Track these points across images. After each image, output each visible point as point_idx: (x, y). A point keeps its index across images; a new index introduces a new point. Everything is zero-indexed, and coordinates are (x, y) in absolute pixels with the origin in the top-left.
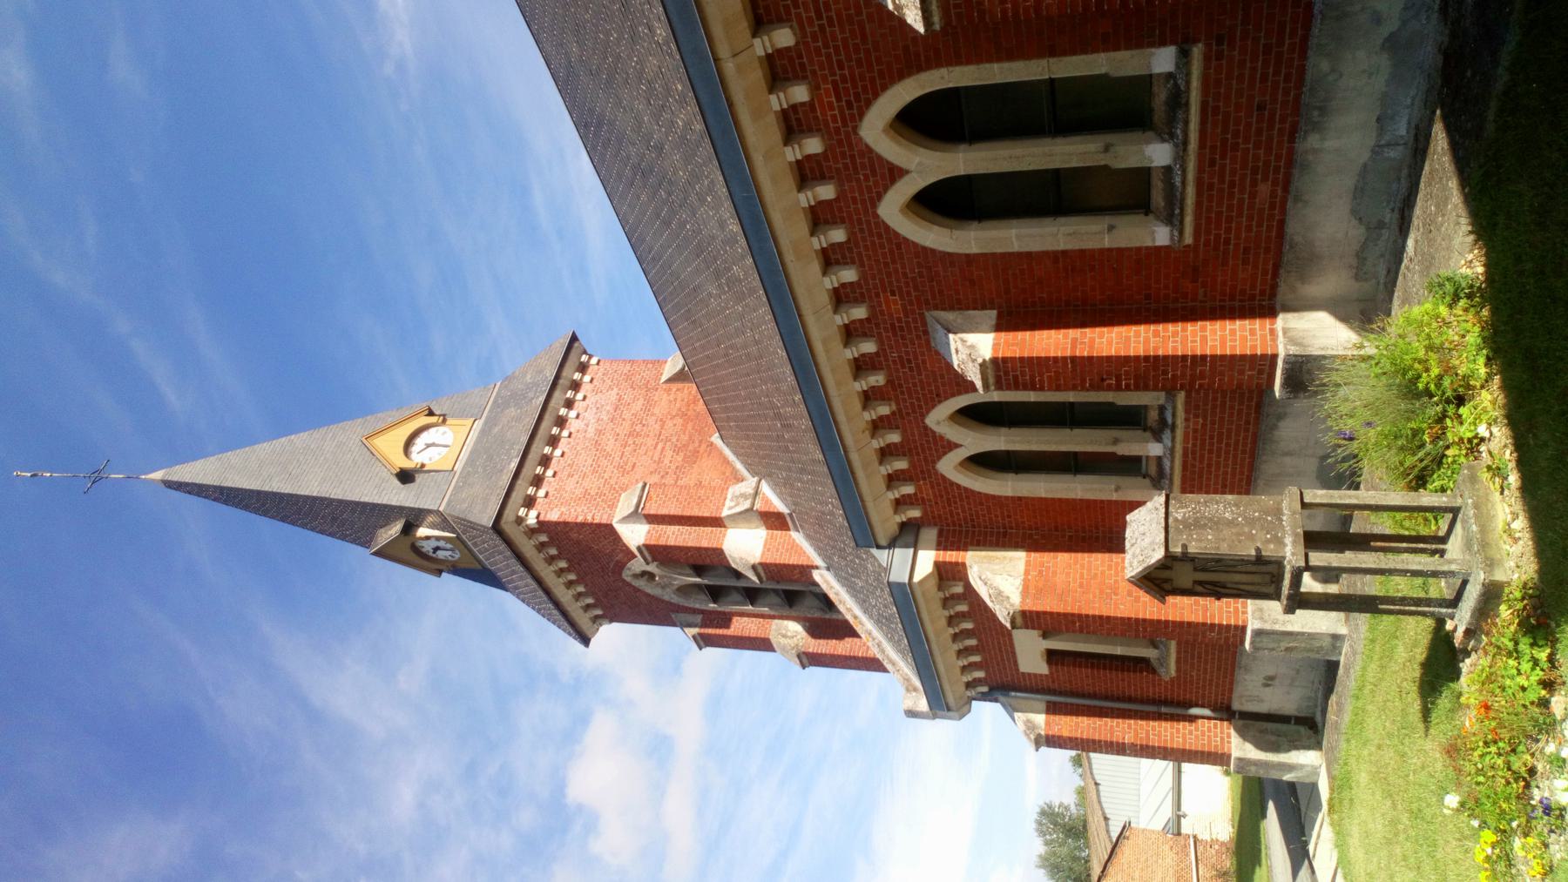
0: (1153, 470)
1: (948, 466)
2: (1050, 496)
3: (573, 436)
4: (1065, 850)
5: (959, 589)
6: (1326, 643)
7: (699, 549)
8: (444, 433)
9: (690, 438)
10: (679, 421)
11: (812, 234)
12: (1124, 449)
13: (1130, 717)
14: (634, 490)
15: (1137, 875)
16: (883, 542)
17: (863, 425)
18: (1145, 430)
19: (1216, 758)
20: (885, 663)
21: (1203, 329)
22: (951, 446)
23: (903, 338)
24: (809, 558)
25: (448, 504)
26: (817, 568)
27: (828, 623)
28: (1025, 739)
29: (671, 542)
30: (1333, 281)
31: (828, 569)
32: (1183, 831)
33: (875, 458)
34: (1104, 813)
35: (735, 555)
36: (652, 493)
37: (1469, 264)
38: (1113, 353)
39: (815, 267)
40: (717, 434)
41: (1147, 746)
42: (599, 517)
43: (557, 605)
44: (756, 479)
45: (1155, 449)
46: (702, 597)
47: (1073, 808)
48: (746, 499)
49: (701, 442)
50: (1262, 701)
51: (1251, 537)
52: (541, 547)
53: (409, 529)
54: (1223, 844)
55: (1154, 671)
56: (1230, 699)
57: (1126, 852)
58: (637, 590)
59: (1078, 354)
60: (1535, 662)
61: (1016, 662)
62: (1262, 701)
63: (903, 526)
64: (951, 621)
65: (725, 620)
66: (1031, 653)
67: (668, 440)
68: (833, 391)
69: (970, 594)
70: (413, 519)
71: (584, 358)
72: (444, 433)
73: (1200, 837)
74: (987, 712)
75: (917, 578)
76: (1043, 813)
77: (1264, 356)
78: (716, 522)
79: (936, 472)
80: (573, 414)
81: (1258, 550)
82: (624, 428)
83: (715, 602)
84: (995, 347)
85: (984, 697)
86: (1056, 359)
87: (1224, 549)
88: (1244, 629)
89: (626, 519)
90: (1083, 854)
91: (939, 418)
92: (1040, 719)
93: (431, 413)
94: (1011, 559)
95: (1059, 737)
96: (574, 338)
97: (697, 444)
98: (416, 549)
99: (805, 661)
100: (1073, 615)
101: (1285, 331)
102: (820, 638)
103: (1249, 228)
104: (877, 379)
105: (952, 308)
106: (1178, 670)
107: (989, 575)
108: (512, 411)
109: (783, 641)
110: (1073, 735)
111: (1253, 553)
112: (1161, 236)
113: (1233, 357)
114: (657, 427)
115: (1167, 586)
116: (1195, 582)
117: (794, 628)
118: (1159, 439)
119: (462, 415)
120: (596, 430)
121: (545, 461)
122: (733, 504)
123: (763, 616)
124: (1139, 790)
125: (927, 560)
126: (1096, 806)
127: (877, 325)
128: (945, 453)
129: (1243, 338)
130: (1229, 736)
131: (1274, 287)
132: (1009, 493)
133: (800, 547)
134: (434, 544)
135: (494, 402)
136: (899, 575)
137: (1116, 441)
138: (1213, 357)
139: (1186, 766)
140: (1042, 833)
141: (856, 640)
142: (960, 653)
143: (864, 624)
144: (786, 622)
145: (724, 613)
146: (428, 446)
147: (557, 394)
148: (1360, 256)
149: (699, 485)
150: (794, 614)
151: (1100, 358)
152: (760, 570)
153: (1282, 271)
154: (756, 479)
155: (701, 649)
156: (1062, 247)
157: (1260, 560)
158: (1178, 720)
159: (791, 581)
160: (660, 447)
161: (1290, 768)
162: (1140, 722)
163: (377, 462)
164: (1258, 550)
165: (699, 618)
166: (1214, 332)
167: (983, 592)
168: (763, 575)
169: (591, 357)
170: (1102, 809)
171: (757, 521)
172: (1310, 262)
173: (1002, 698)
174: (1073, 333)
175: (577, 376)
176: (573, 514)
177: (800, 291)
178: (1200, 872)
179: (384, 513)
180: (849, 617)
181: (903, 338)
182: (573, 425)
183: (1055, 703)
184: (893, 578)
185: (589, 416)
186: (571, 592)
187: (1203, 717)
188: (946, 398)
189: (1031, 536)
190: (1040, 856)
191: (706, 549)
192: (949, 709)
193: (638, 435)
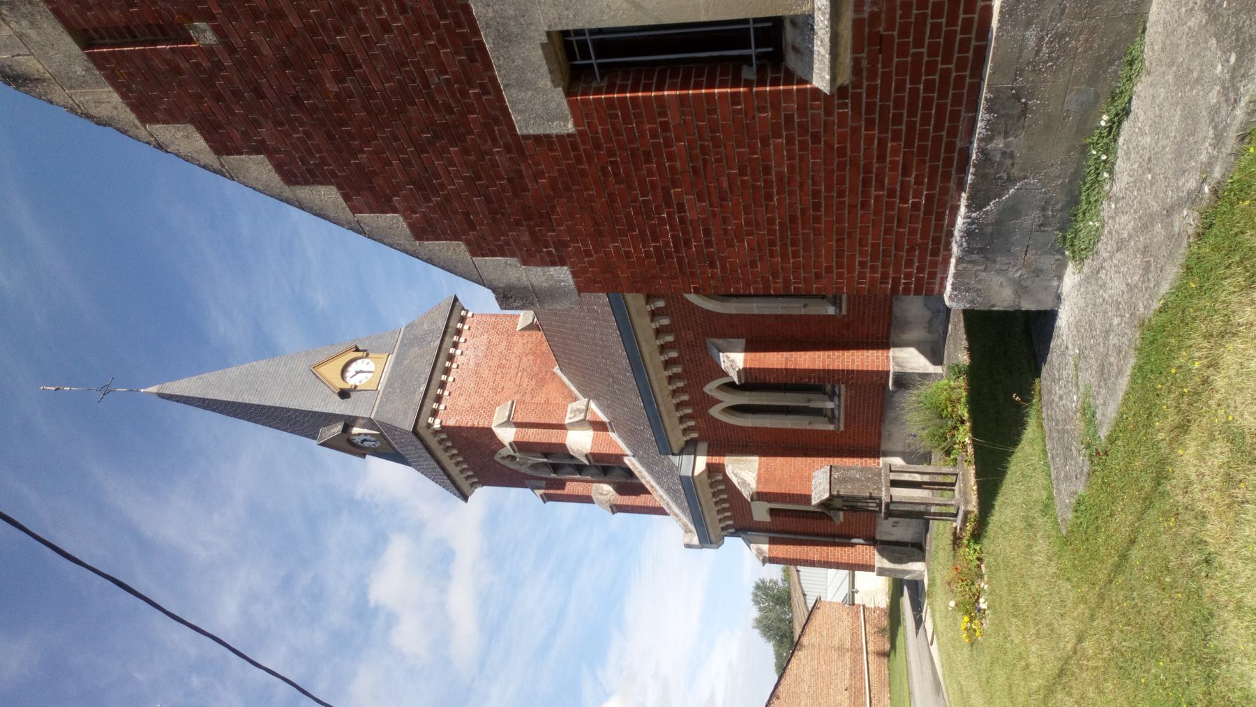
0: (829, 414)
1: (715, 412)
2: (773, 426)
3: (460, 367)
4: (773, 615)
5: (720, 477)
7: (550, 444)
8: (368, 363)
9: (539, 368)
10: (531, 358)
11: (647, 304)
12: (813, 405)
13: (817, 545)
14: (506, 406)
15: (825, 633)
16: (676, 452)
17: (668, 392)
18: (824, 394)
19: (868, 568)
20: (668, 511)
21: (853, 355)
22: (717, 402)
23: (693, 350)
24: (621, 449)
25: (378, 412)
26: (627, 455)
27: (629, 485)
28: (757, 559)
29: (532, 440)
30: (917, 333)
31: (634, 456)
32: (856, 602)
33: (673, 408)
34: (803, 591)
35: (575, 448)
36: (518, 408)
37: (964, 358)
38: (807, 367)
39: (648, 318)
40: (557, 367)
41: (828, 562)
42: (482, 423)
43: (449, 477)
44: (586, 400)
45: (830, 405)
46: (547, 470)
47: (780, 583)
48: (581, 413)
49: (547, 372)
50: (892, 535)
51: (868, 487)
52: (441, 442)
53: (347, 428)
54: (882, 609)
56: (874, 533)
57: (818, 618)
58: (502, 466)
59: (788, 367)
60: (975, 550)
61: (751, 515)
62: (892, 535)
63: (687, 442)
64: (714, 495)
65: (561, 485)
66: (761, 513)
67: (524, 370)
68: (653, 377)
69: (727, 480)
70: (349, 422)
71: (463, 313)
72: (368, 363)
73: (867, 606)
74: (734, 544)
75: (696, 473)
76: (758, 587)
77: (883, 371)
78: (561, 427)
79: (708, 414)
80: (458, 352)
81: (870, 493)
82: (495, 362)
83: (555, 473)
84: (745, 361)
85: (732, 535)
86: (777, 369)
87: (856, 493)
89: (501, 425)
90: (788, 617)
91: (711, 388)
92: (765, 547)
93: (357, 350)
94: (750, 461)
95: (777, 558)
96: (456, 299)
97: (544, 374)
98: (350, 442)
99: (614, 508)
100: (785, 494)
101: (894, 358)
102: (624, 495)
103: (874, 309)
104: (677, 370)
105: (721, 337)
107: (739, 471)
108: (416, 350)
109: (600, 497)
110: (784, 556)
111: (868, 495)
112: (831, 310)
113: (867, 371)
114: (517, 361)
115: (831, 507)
116: (844, 506)
117: (607, 488)
118: (832, 400)
119: (379, 350)
120: (476, 363)
121: (443, 385)
122: (572, 416)
123: (586, 481)
125: (701, 462)
126: (798, 586)
127: (679, 344)
128: (713, 405)
129: (873, 361)
130: (874, 555)
131: (889, 333)
132: (750, 425)
133: (616, 443)
134: (363, 437)
135: (401, 342)
136: (686, 471)
137: (809, 401)
138: (858, 371)
140: (757, 602)
141: (647, 495)
142: (718, 512)
144: (601, 485)
145: (560, 480)
146: (357, 373)
147: (447, 339)
148: (930, 323)
149: (547, 401)
150: (608, 480)
151: (800, 370)
152: (590, 457)
153: (892, 328)
154: (586, 400)
155: (545, 502)
156: (780, 313)
158: (845, 546)
159: (604, 462)
160: (520, 374)
161: (908, 572)
162: (823, 548)
163: (321, 384)
164: (870, 493)
165: (544, 483)
166: (858, 357)
167: (735, 480)
168: (591, 459)
169: (467, 311)
170: (802, 588)
172: (905, 325)
173: (742, 535)
174: (786, 354)
175: (459, 326)
176: (465, 422)
177: (639, 332)
178: (867, 629)
179: (330, 419)
180: (643, 481)
181: (693, 350)
182: (460, 360)
183: (774, 538)
184: (683, 473)
185: (469, 353)
186: (459, 468)
187: (859, 544)
188: (716, 379)
189: (761, 448)
190: (756, 619)
191: (554, 444)
192: (711, 543)
193: (504, 367)
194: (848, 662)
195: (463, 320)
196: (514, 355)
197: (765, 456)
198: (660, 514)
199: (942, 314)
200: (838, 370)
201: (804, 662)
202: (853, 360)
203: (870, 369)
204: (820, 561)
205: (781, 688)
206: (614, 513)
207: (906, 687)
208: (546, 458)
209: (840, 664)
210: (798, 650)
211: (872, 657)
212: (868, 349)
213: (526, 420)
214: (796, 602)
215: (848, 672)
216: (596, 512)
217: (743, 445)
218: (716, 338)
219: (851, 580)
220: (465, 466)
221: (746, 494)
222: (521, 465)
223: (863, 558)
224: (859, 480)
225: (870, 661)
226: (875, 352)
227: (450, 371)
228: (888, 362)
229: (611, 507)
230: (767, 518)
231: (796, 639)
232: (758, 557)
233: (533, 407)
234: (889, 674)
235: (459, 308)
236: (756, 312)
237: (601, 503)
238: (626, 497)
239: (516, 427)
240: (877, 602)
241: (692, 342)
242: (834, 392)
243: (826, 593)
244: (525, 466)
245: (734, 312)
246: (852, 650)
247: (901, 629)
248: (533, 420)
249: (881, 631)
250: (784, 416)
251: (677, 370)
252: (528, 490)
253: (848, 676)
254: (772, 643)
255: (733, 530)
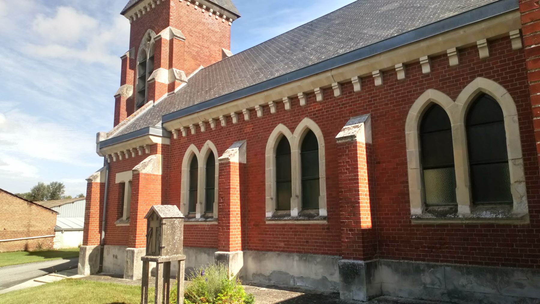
0: (191, 215)
1: (192, 148)
3: (203, 14)
4: (46, 193)
5: (147, 152)
6: (130, 274)
7: (160, 59)
10: (208, 54)
11: (273, 102)
13: (100, 211)
14: (182, 35)
15: (38, 217)
16: (164, 125)
17: (207, 118)
18: (205, 212)
19: (86, 241)
20: (116, 127)
22: (199, 149)
23: (237, 132)
26: (154, 102)
28: (90, 175)
29: (163, 48)
31: (153, 106)
32: (56, 233)
34: (62, 205)
40: (203, 68)
44: (187, 81)
45: (198, 216)
48: (179, 77)
49: (201, 62)
50: (108, 254)
51: (168, 245)
54: (52, 246)
55: (118, 219)
56: (108, 244)
57: (47, 213)
58: (144, 34)
59: (231, 189)
62: (108, 254)
63: (170, 132)
64: (135, 149)
65: (133, 67)
67: (201, 49)
69: (145, 156)
71: (231, 20)
74: (99, 162)
75: (151, 137)
77: (229, 247)
78: (171, 66)
79: (190, 144)
80: (211, 14)
81: (164, 247)
83: (139, 64)
84: (234, 163)
85: (106, 161)
87: (164, 237)
88: (135, 247)
89: (171, 32)
90: (45, 199)
91: (209, 144)
92: (98, 180)
95: (91, 187)
96: (238, 17)
97: (199, 60)
99: (117, 97)
101: (237, 254)
102: (126, 103)
103: (270, 241)
104: (223, 123)
105: (247, 148)
106: (118, 227)
107: (152, 163)
109: (125, 89)
110: (93, 192)
113: (229, 238)
114: (206, 46)
115: (150, 219)
117: (130, 93)
118: (201, 217)
120: (205, 23)
122: (178, 72)
124: (71, 217)
127: (242, 124)
128: (197, 147)
129: (235, 241)
130: (94, 245)
131: (251, 249)
133: (161, 96)
136: (152, 131)
137: (201, 203)
138: (229, 232)
139: (82, 233)
140: (52, 184)
141: (126, 116)
143: (132, 119)
144: (132, 90)
145: (135, 67)
147: (218, 9)
148: (261, 275)
149: (185, 60)
150: (136, 93)
152: (153, 81)
153: (256, 251)
154: (187, 81)
155: (121, 58)
156: (266, 184)
157: (160, 248)
158: (99, 228)
159: (149, 93)
161: (83, 265)
164: (164, 247)
165: (133, 58)
167: (146, 160)
169: (232, 22)
171: (171, 81)
172: (259, 260)
173: (106, 167)
178: (41, 239)
182: (207, 14)
183: (104, 186)
186: (142, 9)
187: (101, 236)
190: (43, 184)
191: (160, 61)
194: (21, 230)
195: (227, 19)
196: (209, 45)
197: (162, 178)
198: (114, 123)
199: (267, 282)
200: (229, 220)
201: (21, 206)
202: (235, 229)
203: (230, 240)
204: (90, 213)
205: (5, 194)
206: (115, 96)
207: (6, 264)
208: (150, 58)
209: (20, 225)
210: (28, 203)
211: (24, 242)
212: (242, 237)
213: (174, 46)
214: (55, 202)
215: (15, 230)
216: (115, 86)
217: (168, 165)
218: (247, 146)
219: (70, 229)
220: (144, 13)
221: (136, 167)
222: (145, 45)
223: (92, 238)
224: (173, 238)
225: (22, 241)
226: (240, 242)
227: (201, 8)
228: (234, 250)
229: (119, 95)
230: (118, 180)
231: (34, 202)
232: (92, 176)
233: (182, 51)
234: (14, 252)
235: (234, 19)
236: (267, 169)
237: (121, 89)
238: (125, 103)
239: (170, 40)
240: (57, 243)
241: (244, 131)
242: (208, 218)
243: (61, 217)
244: (144, 46)
245: (266, 156)
246: (29, 231)
247: (42, 258)
248: (175, 49)
249: (40, 246)
250: (189, 189)
251: (223, 123)
252: (128, 49)
253: (13, 230)
254: (30, 192)
255: (109, 161)
